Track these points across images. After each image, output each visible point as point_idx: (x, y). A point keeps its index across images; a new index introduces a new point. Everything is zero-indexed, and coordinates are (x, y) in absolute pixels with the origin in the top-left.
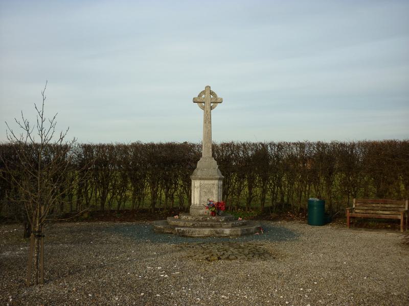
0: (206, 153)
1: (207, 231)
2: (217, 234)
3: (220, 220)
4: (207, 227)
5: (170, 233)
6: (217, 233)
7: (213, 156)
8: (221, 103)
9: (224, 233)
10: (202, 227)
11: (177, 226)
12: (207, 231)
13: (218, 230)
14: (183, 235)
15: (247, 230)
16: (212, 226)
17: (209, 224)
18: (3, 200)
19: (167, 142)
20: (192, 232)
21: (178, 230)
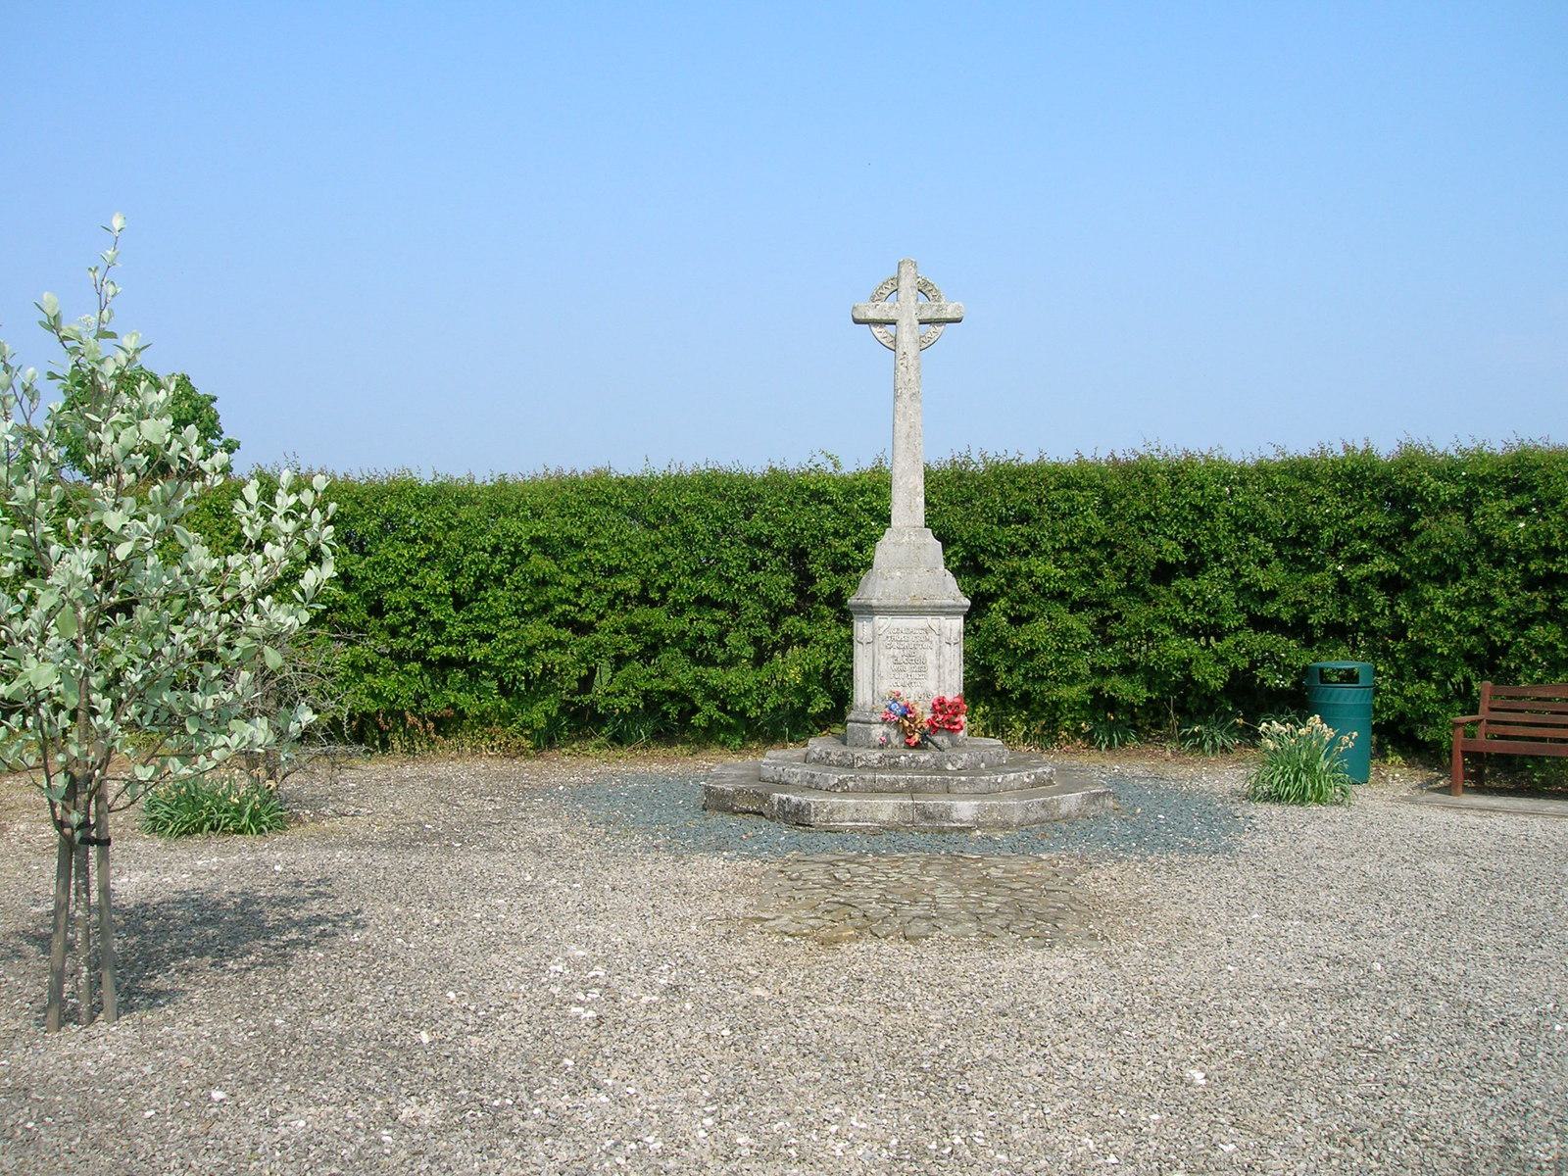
0: (908, 504)
1: (886, 809)
2: (927, 818)
3: (949, 767)
4: (893, 790)
5: (755, 813)
6: (927, 816)
7: (929, 523)
8: (958, 321)
9: (955, 815)
10: (875, 790)
11: (782, 784)
12: (886, 809)
13: (931, 802)
14: (797, 817)
15: (1044, 805)
16: (913, 789)
17: (902, 779)
18: (1372, 571)
19: (1467, 444)
20: (831, 812)
21: (781, 802)
